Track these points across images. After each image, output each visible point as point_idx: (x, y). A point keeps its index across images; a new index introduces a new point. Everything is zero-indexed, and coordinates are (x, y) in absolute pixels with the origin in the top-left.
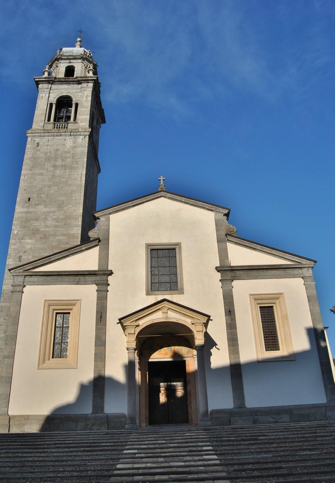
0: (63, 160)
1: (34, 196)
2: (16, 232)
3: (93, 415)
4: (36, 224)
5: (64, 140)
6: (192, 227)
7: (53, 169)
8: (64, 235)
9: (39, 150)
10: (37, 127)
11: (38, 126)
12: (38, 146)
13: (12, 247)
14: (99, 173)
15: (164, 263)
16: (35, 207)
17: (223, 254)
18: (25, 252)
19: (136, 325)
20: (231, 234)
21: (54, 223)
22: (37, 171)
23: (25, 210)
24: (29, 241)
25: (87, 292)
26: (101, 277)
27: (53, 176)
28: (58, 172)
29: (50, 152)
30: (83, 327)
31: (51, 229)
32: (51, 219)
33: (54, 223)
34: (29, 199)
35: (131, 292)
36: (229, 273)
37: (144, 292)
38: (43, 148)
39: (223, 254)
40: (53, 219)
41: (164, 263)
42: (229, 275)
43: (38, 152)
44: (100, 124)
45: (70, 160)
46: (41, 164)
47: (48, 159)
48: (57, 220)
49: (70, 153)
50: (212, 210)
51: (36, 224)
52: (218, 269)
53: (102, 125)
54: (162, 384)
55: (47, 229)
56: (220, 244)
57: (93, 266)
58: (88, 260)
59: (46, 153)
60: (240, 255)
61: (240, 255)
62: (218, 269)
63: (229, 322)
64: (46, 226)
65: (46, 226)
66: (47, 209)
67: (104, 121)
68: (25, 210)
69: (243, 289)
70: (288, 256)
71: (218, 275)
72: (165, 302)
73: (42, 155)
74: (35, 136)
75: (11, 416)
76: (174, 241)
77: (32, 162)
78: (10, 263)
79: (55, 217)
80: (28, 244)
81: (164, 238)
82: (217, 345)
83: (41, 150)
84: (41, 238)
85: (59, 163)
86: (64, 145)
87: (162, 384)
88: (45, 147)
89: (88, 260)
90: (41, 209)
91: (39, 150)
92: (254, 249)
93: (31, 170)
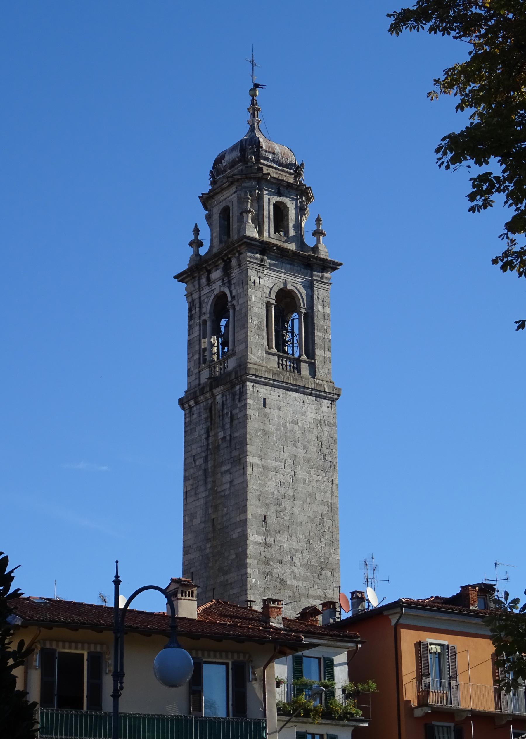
27: (294, 477)
31: (300, 583)
33: (303, 571)
55: (295, 583)
74: (258, 382)
85: (301, 452)
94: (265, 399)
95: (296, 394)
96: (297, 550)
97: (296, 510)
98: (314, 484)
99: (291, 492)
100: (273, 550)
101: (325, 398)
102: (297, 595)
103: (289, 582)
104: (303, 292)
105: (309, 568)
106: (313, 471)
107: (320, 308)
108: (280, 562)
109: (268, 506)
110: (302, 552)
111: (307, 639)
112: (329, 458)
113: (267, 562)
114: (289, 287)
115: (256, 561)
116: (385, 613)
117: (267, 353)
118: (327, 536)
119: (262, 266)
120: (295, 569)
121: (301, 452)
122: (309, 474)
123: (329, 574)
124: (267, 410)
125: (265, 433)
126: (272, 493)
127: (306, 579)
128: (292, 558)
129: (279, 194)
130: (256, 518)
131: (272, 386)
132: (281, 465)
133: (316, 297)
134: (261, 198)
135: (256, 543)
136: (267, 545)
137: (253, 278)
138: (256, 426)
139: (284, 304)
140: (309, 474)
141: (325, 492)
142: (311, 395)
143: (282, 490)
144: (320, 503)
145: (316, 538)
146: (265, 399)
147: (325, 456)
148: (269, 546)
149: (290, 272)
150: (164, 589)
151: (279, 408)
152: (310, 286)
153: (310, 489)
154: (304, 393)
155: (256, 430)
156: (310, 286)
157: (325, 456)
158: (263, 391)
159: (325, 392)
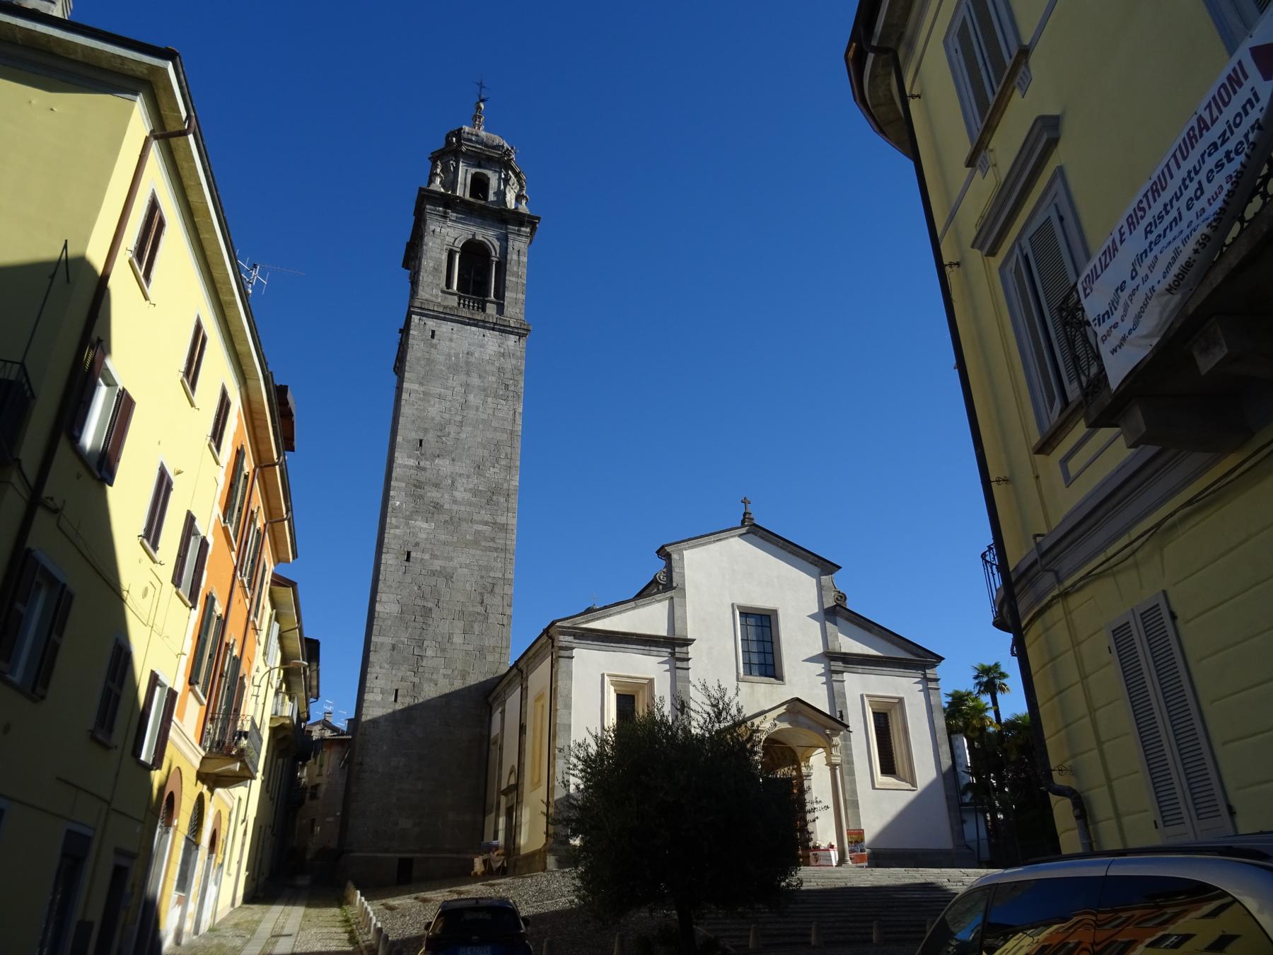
1: (430, 438)
4: (432, 494)
6: (793, 595)
8: (486, 523)
9: (434, 346)
10: (427, 296)
12: (433, 336)
13: (392, 531)
19: (946, 737)
20: (835, 612)
23: (412, 462)
24: (425, 525)
26: (673, 646)
27: (465, 405)
29: (457, 356)
31: (463, 508)
33: (468, 496)
38: (444, 346)
41: (761, 639)
42: (838, 665)
45: (494, 379)
47: (454, 369)
48: (476, 492)
51: (432, 494)
54: (547, 893)
55: (455, 507)
57: (660, 628)
58: (650, 618)
59: (449, 355)
65: (455, 502)
68: (412, 462)
73: (442, 358)
74: (426, 316)
78: (390, 562)
79: (471, 486)
81: (760, 601)
85: (475, 381)
86: (482, 346)
87: (547, 893)
89: (650, 618)
90: (444, 465)
93: (421, 384)
94: (433, 332)
95: (473, 328)
96: (461, 475)
97: (463, 436)
98: (491, 411)
99: (459, 418)
100: (428, 474)
101: (512, 333)
102: (456, 520)
103: (447, 506)
104: (497, 244)
105: (476, 492)
106: (490, 400)
107: (515, 257)
108: (437, 485)
109: (426, 430)
110: (468, 477)
111: (1099, 649)
112: (511, 388)
113: (419, 485)
114: (479, 238)
115: (404, 485)
116: (945, 841)
117: (443, 292)
118: (503, 463)
119: (445, 217)
120: (457, 494)
121: (475, 381)
122: (485, 402)
123: (502, 500)
124: (435, 341)
125: (430, 361)
126: (433, 419)
127: (470, 504)
128: (453, 482)
129: (479, 166)
130: (409, 441)
131: (444, 319)
132: (449, 392)
133: (510, 249)
134: (456, 169)
135: (406, 466)
136: (418, 468)
137: (432, 228)
138: (419, 355)
139: (474, 254)
140: (485, 402)
141: (504, 419)
142: (493, 329)
143: (447, 416)
144: (495, 429)
145: (488, 464)
146: (433, 332)
147: (507, 386)
148: (424, 469)
149: (482, 226)
150: (1011, 636)
151: (451, 340)
152: (504, 240)
153: (485, 417)
154: (484, 327)
155: (418, 359)
156: (504, 240)
157: (507, 386)
158: (431, 323)
159: (1076, 644)
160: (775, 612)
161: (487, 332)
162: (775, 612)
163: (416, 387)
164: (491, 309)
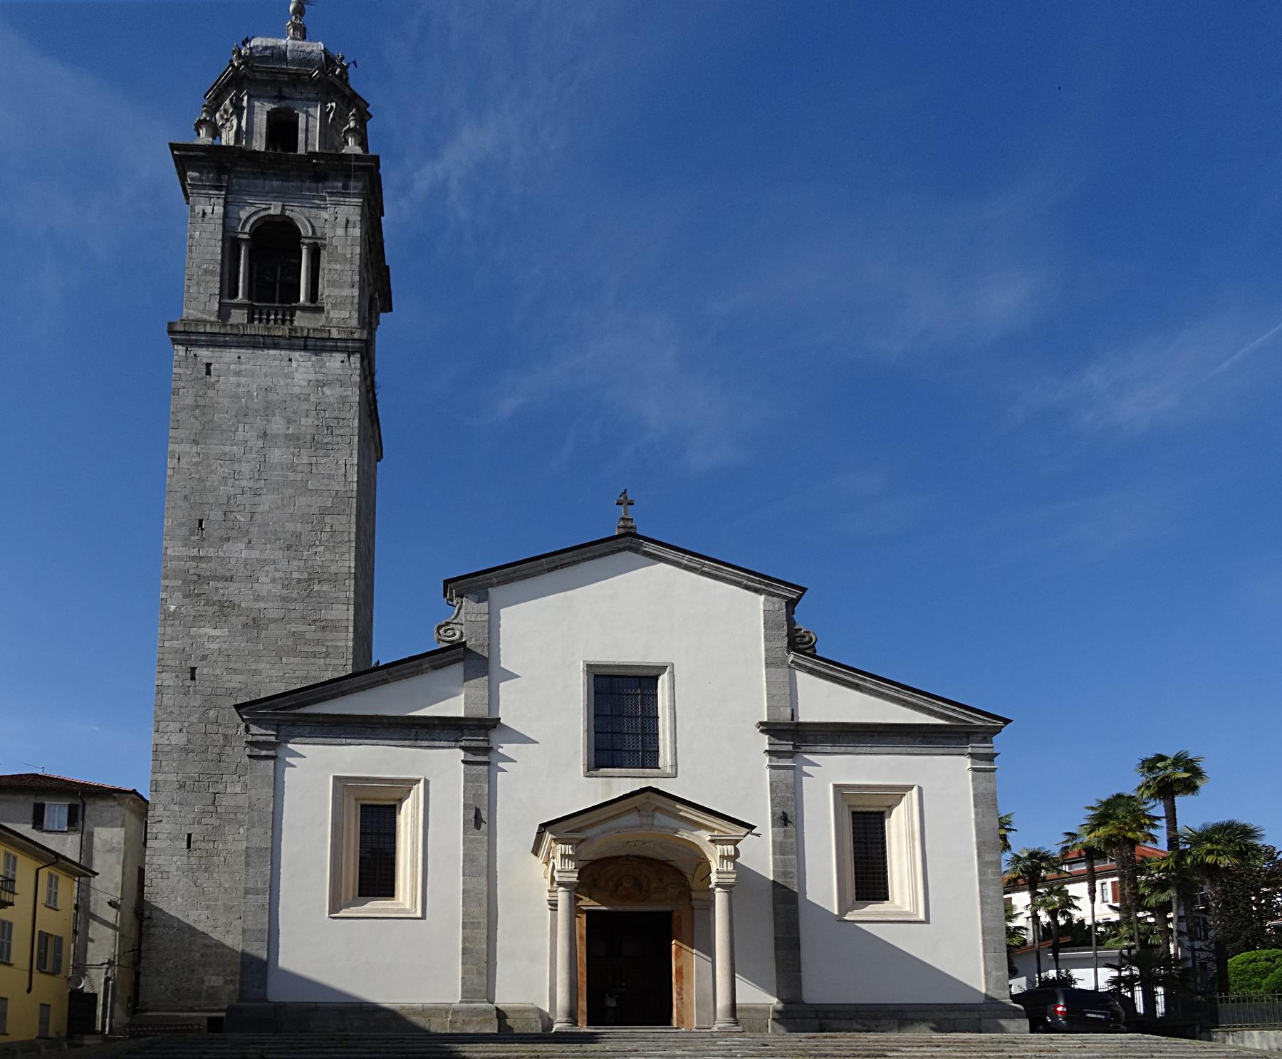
0: (289, 421)
2: (172, 608)
3: (465, 1005)
4: (231, 590)
5: (285, 363)
7: (260, 443)
9: (212, 386)
11: (203, 312)
12: (208, 373)
14: (378, 460)
15: (622, 710)
16: (221, 547)
17: (786, 693)
18: (204, 658)
21: (278, 590)
22: (215, 449)
25: (444, 766)
28: (277, 455)
30: (425, 839)
31: (270, 605)
32: (267, 580)
33: (278, 590)
34: (201, 522)
35: (552, 771)
36: (792, 737)
37: (581, 769)
39: (786, 693)
40: (273, 580)
41: (622, 710)
43: (211, 393)
44: (378, 315)
46: (224, 427)
47: (243, 413)
49: (307, 400)
50: (756, 591)
51: (231, 590)
52: (768, 728)
53: (383, 317)
56: (772, 670)
59: (237, 397)
60: (822, 701)
61: (822, 701)
62: (768, 728)
63: (779, 840)
64: (258, 598)
65: (258, 598)
66: (256, 554)
67: (388, 307)
69: (829, 772)
70: (937, 706)
71: (970, 773)
72: (648, 794)
75: (514, 1011)
76: (654, 659)
77: (196, 418)
79: (278, 575)
80: (212, 638)
81: (627, 651)
82: (173, 147)
83: (220, 386)
84: (245, 626)
85: (277, 425)
88: (232, 379)
90: (237, 550)
91: (212, 386)
92: (856, 687)
93: (195, 442)
95: (272, 352)
101: (335, 349)
124: (213, 379)
135: (179, 558)
146: (208, 365)
158: (205, 354)
160: (590, 667)
161: (297, 355)
162: (590, 667)
163: (184, 448)
164: (301, 320)
